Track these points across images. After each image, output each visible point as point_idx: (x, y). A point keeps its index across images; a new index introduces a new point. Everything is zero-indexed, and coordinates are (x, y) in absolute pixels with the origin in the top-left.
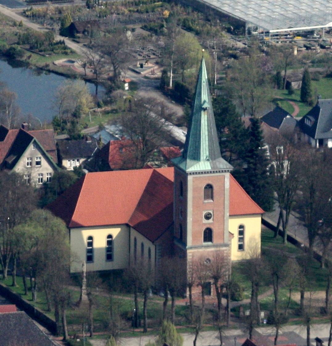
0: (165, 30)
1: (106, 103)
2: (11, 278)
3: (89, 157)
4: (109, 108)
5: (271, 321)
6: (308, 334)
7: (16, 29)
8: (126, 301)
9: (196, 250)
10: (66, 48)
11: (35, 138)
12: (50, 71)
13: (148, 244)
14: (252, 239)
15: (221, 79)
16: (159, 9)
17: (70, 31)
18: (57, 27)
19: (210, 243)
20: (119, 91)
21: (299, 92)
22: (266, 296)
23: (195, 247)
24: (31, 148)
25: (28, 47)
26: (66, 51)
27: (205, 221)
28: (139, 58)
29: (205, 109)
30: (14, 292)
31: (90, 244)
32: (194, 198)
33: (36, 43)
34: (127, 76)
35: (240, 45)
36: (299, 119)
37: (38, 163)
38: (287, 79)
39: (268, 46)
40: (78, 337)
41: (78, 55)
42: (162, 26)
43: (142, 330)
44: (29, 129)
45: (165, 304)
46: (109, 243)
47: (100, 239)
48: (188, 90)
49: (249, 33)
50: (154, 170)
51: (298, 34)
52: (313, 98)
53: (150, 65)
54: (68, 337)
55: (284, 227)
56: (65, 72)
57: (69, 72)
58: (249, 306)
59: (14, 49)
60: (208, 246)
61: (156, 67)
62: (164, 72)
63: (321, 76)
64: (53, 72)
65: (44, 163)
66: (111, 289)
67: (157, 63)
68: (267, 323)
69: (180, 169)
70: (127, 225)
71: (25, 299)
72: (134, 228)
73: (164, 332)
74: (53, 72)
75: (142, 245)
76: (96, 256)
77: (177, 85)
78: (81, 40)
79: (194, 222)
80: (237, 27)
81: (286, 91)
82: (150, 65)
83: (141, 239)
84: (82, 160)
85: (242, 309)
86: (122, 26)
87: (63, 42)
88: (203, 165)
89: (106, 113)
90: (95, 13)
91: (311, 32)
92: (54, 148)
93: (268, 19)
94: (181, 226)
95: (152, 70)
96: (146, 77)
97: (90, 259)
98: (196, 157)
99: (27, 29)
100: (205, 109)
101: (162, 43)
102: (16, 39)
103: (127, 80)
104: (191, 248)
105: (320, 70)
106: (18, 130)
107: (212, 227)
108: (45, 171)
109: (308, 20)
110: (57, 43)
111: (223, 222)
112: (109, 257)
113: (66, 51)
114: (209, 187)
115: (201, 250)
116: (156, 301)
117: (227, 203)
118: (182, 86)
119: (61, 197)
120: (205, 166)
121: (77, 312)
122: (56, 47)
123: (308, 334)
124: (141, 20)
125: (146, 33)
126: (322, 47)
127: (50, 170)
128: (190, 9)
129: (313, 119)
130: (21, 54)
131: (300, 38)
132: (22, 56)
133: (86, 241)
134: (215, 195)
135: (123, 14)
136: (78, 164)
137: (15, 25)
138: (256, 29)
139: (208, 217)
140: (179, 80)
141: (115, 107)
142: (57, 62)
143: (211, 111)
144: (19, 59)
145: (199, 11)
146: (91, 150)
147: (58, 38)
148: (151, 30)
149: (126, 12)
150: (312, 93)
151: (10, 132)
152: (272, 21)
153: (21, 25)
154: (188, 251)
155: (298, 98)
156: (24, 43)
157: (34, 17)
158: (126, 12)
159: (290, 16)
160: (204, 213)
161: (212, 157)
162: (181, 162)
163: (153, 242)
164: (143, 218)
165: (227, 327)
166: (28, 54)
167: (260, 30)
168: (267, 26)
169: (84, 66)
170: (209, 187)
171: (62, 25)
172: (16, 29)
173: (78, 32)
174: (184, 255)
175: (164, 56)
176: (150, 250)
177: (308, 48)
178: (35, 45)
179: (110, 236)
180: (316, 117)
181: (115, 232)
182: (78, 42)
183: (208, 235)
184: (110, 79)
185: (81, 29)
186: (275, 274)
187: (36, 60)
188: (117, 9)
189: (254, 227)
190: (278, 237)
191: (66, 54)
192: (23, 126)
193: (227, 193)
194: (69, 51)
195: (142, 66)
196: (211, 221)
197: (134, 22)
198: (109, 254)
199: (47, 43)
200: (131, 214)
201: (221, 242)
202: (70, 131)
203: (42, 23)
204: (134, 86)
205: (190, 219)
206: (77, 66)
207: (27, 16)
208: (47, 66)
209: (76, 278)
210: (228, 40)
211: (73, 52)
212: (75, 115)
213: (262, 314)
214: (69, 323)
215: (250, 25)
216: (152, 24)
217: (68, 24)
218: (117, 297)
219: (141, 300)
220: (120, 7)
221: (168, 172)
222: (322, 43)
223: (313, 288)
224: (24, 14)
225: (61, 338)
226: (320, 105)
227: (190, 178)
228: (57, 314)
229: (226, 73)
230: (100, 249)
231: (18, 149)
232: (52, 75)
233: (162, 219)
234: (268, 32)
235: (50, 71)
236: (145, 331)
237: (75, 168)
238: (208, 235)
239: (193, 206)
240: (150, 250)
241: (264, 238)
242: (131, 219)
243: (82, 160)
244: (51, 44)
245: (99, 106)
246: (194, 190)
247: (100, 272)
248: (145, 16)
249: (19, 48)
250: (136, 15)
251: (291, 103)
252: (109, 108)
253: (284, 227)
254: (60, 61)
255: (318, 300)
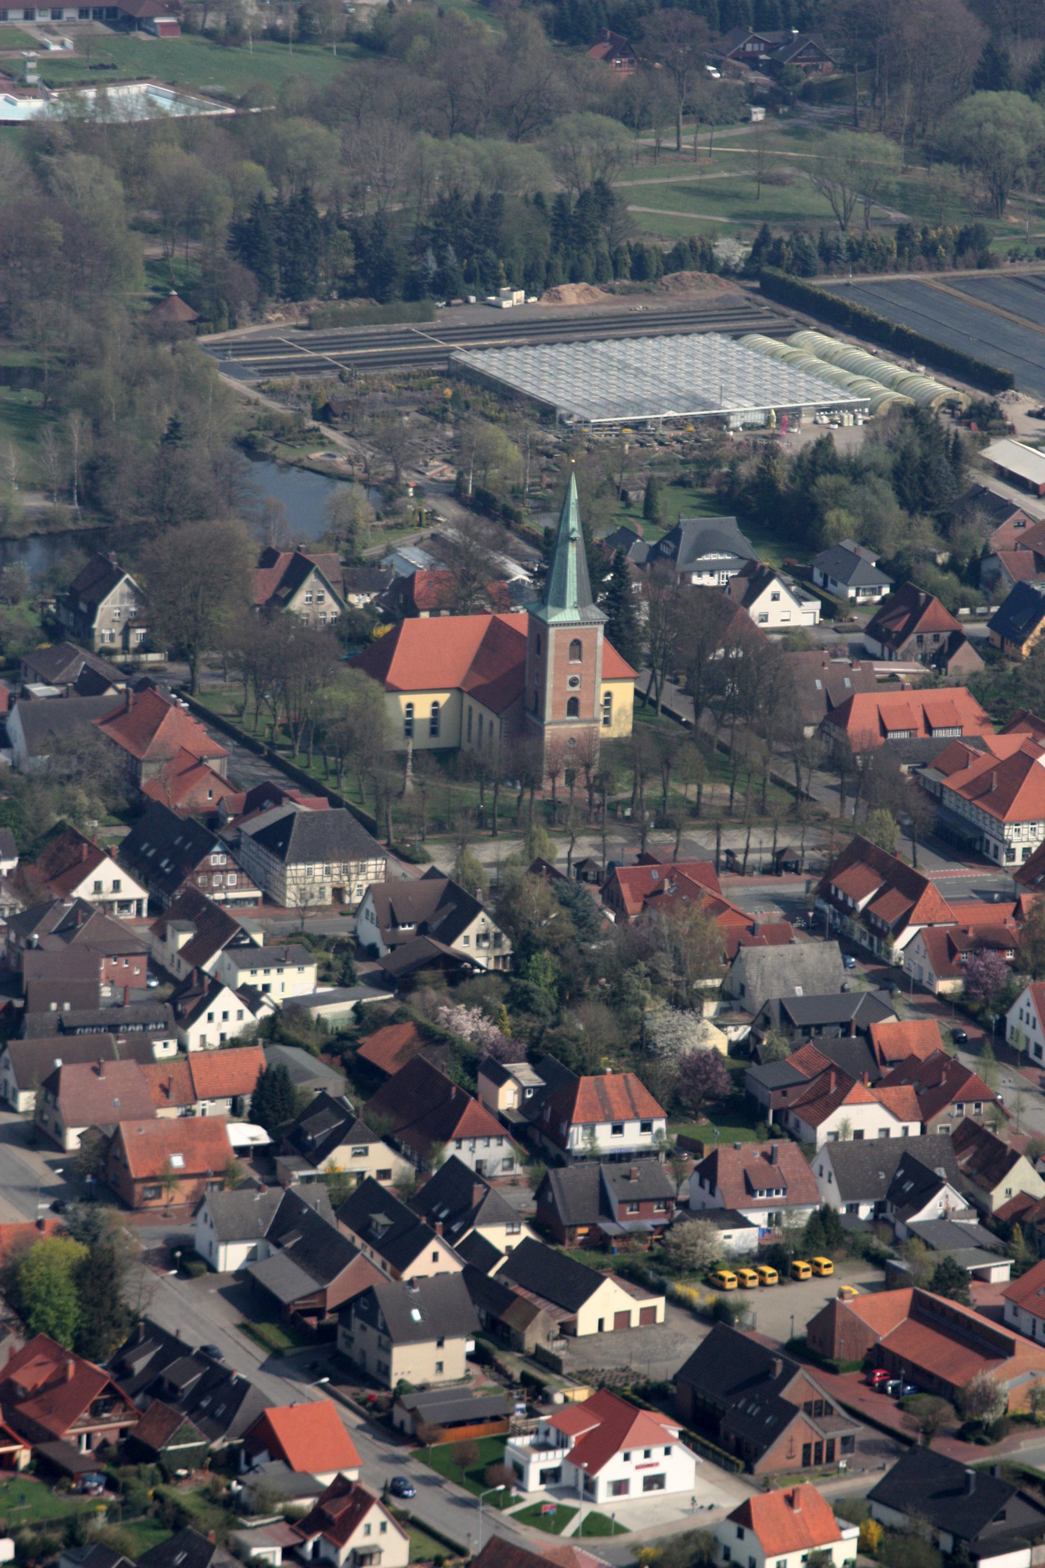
0: (451, 416)
1: (387, 514)
2: (304, 755)
3: (384, 591)
4: (391, 522)
5: (663, 824)
6: (718, 844)
7: (250, 409)
8: (470, 793)
9: (557, 728)
10: (322, 437)
11: (317, 566)
12: (304, 468)
13: (489, 716)
14: (621, 711)
15: (533, 484)
16: (438, 386)
17: (325, 414)
18: (307, 407)
19: (575, 718)
20: (403, 499)
21: (641, 505)
22: (652, 790)
23: (556, 723)
24: (311, 579)
25: (271, 434)
26: (322, 442)
27: (570, 689)
28: (421, 453)
29: (573, 540)
30: (312, 777)
31: (409, 713)
32: (556, 657)
33: (282, 428)
34: (410, 479)
35: (551, 438)
36: (653, 543)
37: (320, 598)
38: (623, 488)
39: (589, 441)
40: (407, 841)
41: (339, 448)
42: (445, 410)
43: (490, 833)
44: (308, 552)
45: (520, 799)
46: (435, 712)
47: (423, 709)
48: (494, 500)
49: (561, 422)
50: (494, 618)
51: (625, 425)
52: (661, 514)
53: (436, 463)
54: (393, 841)
55: (657, 694)
56: (324, 470)
57: (330, 471)
58: (630, 803)
59: (254, 437)
60: (573, 722)
61: (445, 466)
62: (460, 474)
63: (665, 484)
64: (308, 469)
65: (329, 599)
66: (453, 776)
67: (445, 461)
68: (656, 827)
69: (538, 618)
70: (459, 689)
71: (329, 784)
72: (469, 693)
73: (532, 840)
74: (308, 469)
75: (481, 717)
76: (416, 729)
77: (479, 494)
78: (339, 426)
79: (555, 689)
80: (546, 413)
81: (622, 504)
82: (436, 463)
83: (478, 708)
84: (374, 595)
85: (620, 808)
86: (392, 408)
87: (317, 430)
88: (569, 614)
89: (389, 528)
90: (354, 390)
91: (644, 423)
92: (340, 579)
93: (585, 404)
94: (536, 693)
95: (441, 471)
96: (433, 480)
97: (409, 733)
98: (561, 604)
99: (266, 409)
100: (573, 540)
101: (450, 433)
102: (253, 423)
103: (412, 484)
104: (550, 724)
105: (663, 474)
106: (292, 554)
107: (578, 696)
108: (330, 608)
109: (638, 406)
110: (310, 430)
111: (593, 689)
112: (434, 732)
113: (322, 442)
114: (577, 643)
115: (563, 727)
116: (510, 794)
117: (599, 665)
118: (487, 495)
119: (367, 649)
120: (570, 615)
121: (404, 805)
122: (309, 435)
123: (718, 844)
124: (414, 401)
125: (425, 419)
126: (661, 444)
127: (336, 608)
128: (479, 388)
129: (672, 546)
130: (263, 444)
131: (629, 430)
132: (264, 446)
133: (404, 709)
134: (584, 654)
135: (391, 392)
136: (368, 600)
137: (249, 403)
138: (570, 416)
139: (573, 683)
140: (480, 484)
141: (400, 520)
142: (313, 456)
143: (581, 543)
144: (260, 450)
145: (491, 391)
146: (386, 582)
147: (311, 423)
148: (430, 414)
149: (394, 389)
150: (659, 507)
151: (282, 555)
152: (590, 406)
153: (257, 403)
154: (547, 728)
155: (641, 514)
156: (265, 429)
157: (272, 392)
158: (394, 389)
159: (615, 400)
160: (569, 677)
161: (580, 604)
162: (539, 609)
163: (498, 714)
164: (481, 681)
165: (611, 833)
166: (273, 444)
167: (576, 418)
168: (586, 414)
169: (350, 462)
170: (577, 643)
171: (313, 405)
172: (250, 409)
173: (336, 416)
174: (541, 731)
175: (457, 451)
176: (491, 724)
177: (642, 445)
178: (282, 432)
179: (435, 704)
180: (677, 542)
181: (443, 698)
182: (336, 429)
183: (573, 707)
184: (388, 481)
185: (338, 410)
186: (667, 763)
187: (284, 452)
188: (382, 385)
189: (623, 694)
190: (648, 707)
191: (323, 445)
192: (299, 549)
193: (600, 652)
194: (326, 441)
195: (426, 464)
196: (577, 688)
197: (405, 403)
198: (434, 725)
199: (296, 430)
200: (463, 675)
201: (588, 716)
202: (346, 552)
203: (283, 402)
204: (419, 491)
205: (550, 685)
206: (341, 461)
207: (263, 392)
208: (300, 460)
209: (401, 758)
210: (538, 433)
211: (332, 443)
212: (351, 531)
213: (647, 814)
214: (395, 821)
215: (563, 412)
216: (431, 406)
217: (321, 405)
218: (457, 787)
219: (489, 793)
220: (385, 382)
221: (518, 619)
222: (660, 438)
223: (714, 779)
224: (258, 388)
225: (385, 842)
226: (682, 527)
227: (552, 631)
228: (378, 810)
229: (541, 477)
230: (423, 720)
231: (293, 579)
232: (307, 473)
233: (509, 679)
234: (587, 422)
235: (304, 468)
236: (494, 835)
237: (366, 605)
238: (573, 707)
239: (555, 668)
240: (491, 724)
241: (637, 709)
242: (465, 682)
243: (374, 595)
244: (302, 431)
245: (378, 518)
246: (558, 647)
247: (429, 750)
248: (418, 395)
249: (259, 435)
250: (409, 393)
251: (632, 520)
252: (391, 522)
253: (657, 694)
254: (317, 455)
255: (721, 797)
